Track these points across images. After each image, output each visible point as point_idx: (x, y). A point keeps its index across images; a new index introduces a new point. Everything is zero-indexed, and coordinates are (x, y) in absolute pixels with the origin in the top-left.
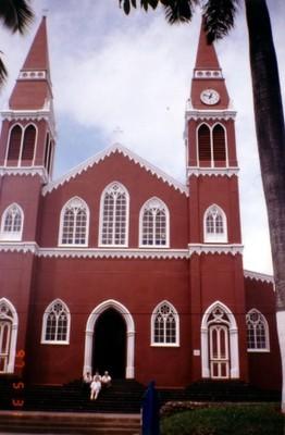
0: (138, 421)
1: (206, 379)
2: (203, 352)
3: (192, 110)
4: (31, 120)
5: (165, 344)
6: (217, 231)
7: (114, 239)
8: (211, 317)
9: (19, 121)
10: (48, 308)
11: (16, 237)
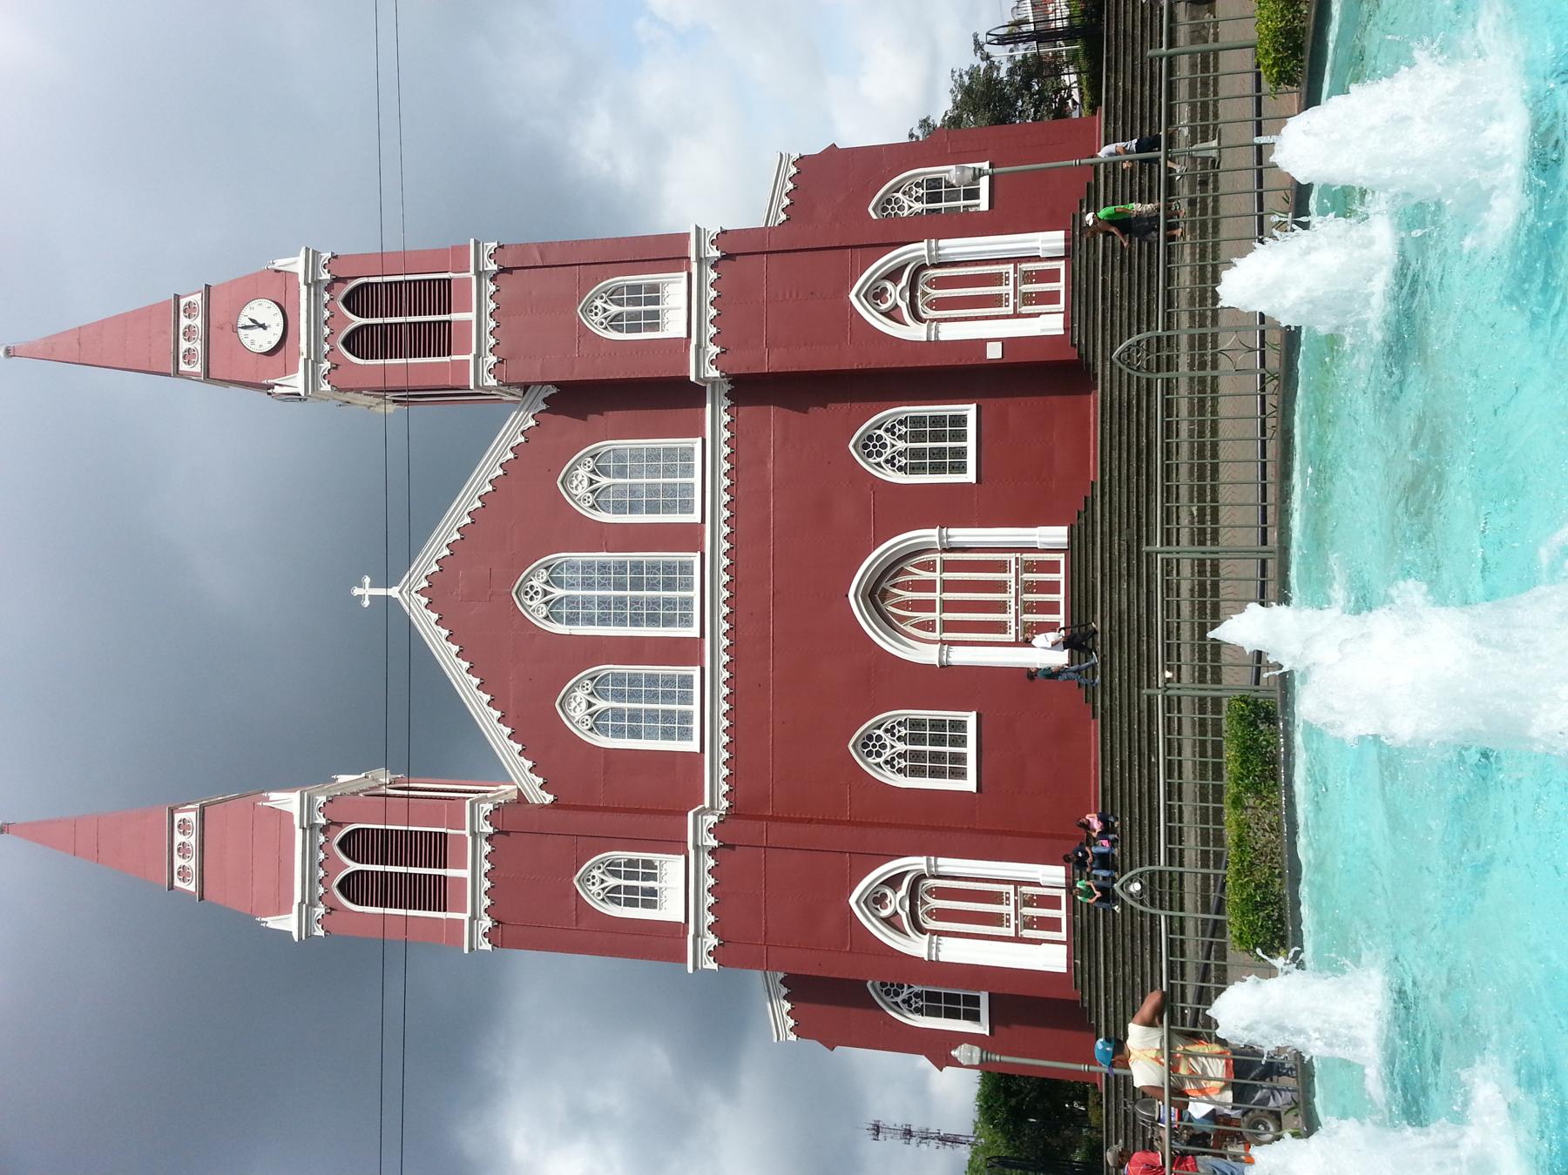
1: (1070, 957)
5: (971, 444)
6: (656, 301)
11: (671, 869)
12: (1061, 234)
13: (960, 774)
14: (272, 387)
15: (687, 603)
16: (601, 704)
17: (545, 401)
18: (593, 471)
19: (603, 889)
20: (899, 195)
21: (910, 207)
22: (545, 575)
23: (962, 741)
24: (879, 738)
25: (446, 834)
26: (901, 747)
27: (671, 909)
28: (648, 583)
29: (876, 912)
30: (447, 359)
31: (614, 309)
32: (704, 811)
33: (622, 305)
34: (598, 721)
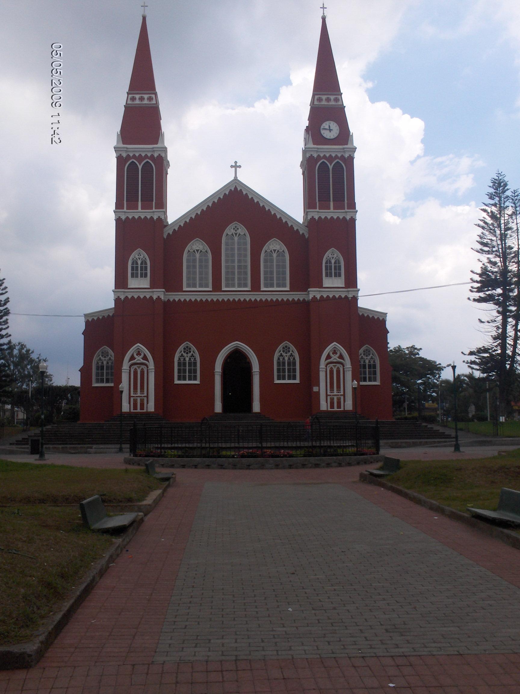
2: (322, 388)
3: (121, 145)
4: (146, 156)
9: (325, 157)
10: (178, 351)
11: (145, 283)
12: (153, 410)
17: (303, 234)
18: (278, 251)
19: (137, 259)
20: (371, 355)
21: (367, 359)
22: (242, 234)
24: (190, 352)
27: (133, 283)
29: (135, 352)
33: (141, 264)
34: (269, 254)
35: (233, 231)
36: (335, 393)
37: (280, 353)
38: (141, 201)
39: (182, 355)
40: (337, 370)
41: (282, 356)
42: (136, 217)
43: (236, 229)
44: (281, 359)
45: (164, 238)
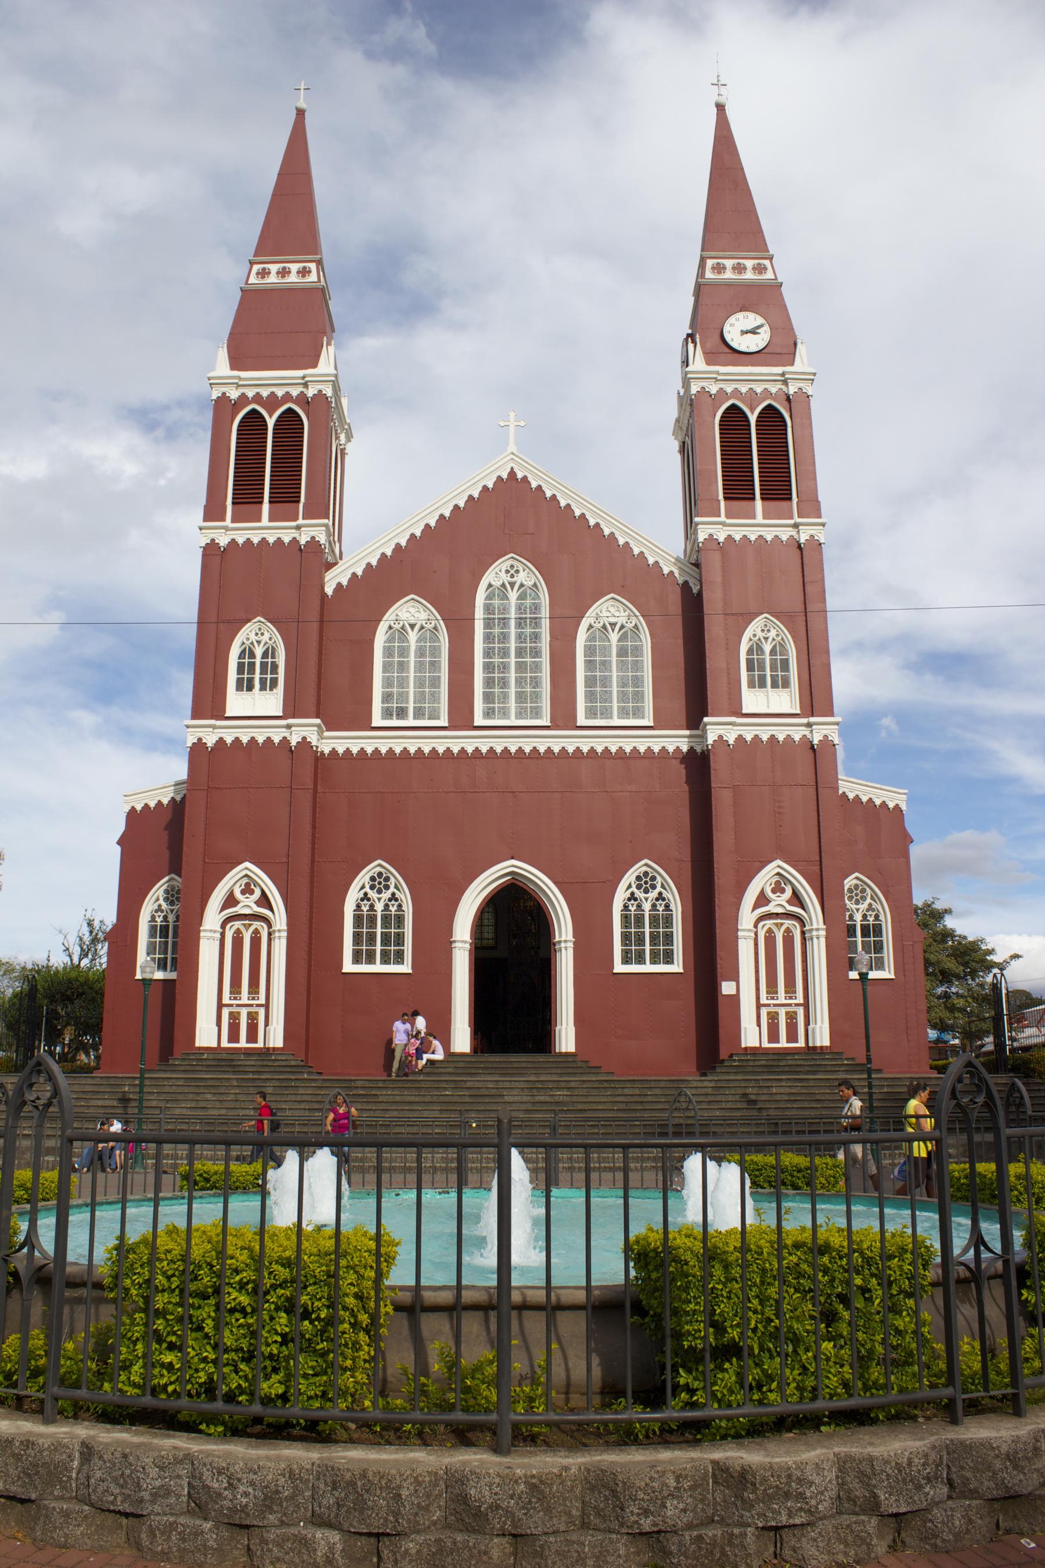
0: (965, 1169)
4: (767, 393)
5: (648, 968)
6: (774, 685)
7: (512, 704)
8: (230, 901)
9: (257, 398)
11: (271, 702)
12: (826, 1042)
13: (357, 959)
14: (694, 342)
15: (505, 714)
16: (413, 636)
19: (252, 643)
20: (869, 900)
21: (858, 910)
23: (385, 960)
25: (298, 502)
26: (379, 907)
27: (236, 703)
28: (521, 678)
30: (721, 496)
31: (767, 648)
32: (320, 733)
33: (771, 654)
34: (399, 634)
35: (506, 578)
36: (782, 1000)
37: (630, 891)
38: (270, 502)
39: (366, 897)
40: (252, 937)
41: (636, 899)
42: (256, 540)
43: (512, 572)
44: (365, 909)
45: (324, 595)
